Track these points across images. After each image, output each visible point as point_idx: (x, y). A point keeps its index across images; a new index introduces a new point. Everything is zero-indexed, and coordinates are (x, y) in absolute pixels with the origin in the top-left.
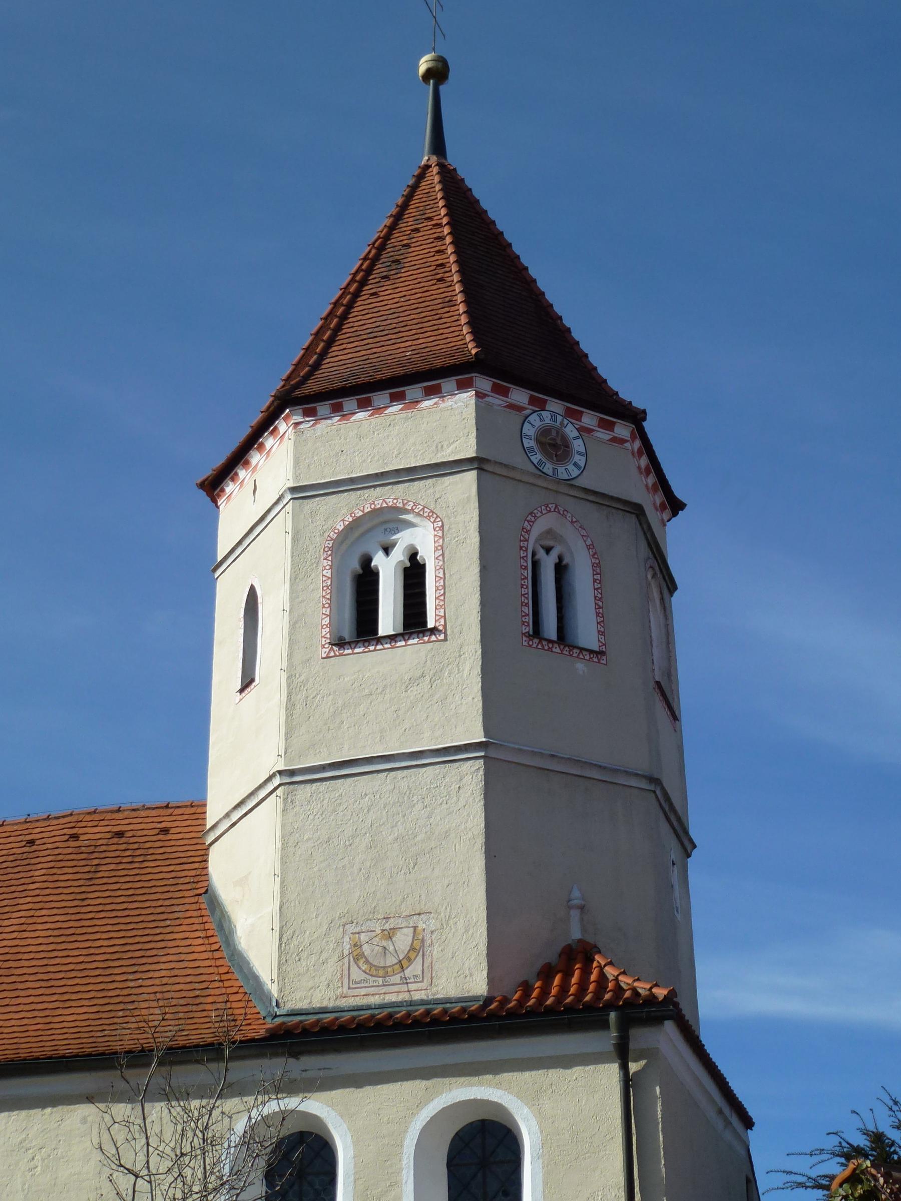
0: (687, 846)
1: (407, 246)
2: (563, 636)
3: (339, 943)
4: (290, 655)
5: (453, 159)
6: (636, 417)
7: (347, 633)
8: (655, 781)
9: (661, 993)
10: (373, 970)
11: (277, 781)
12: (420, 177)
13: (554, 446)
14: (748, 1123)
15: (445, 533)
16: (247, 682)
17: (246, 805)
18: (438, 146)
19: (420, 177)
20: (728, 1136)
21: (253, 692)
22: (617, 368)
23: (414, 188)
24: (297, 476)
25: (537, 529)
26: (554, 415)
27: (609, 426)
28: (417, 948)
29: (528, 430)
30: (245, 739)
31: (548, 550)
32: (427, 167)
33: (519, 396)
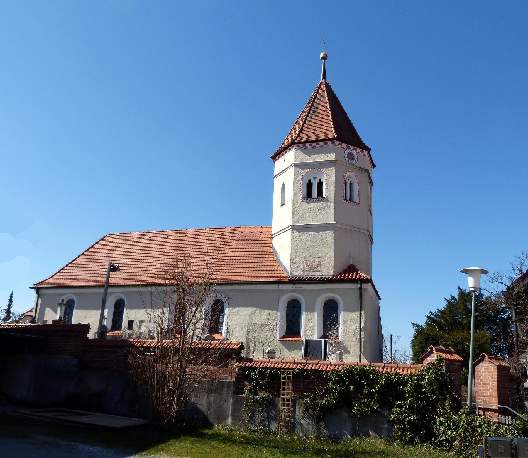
0: (372, 242)
1: (318, 104)
2: (351, 200)
3: (303, 262)
4: (293, 201)
5: (328, 80)
6: (368, 150)
7: (305, 196)
8: (368, 231)
9: (369, 277)
10: (310, 268)
11: (290, 228)
12: (321, 85)
13: (351, 157)
14: (380, 299)
15: (329, 179)
16: (282, 205)
17: (282, 231)
18: (324, 77)
19: (321, 85)
20: (376, 302)
21: (283, 207)
22: (366, 142)
23: (319, 88)
24: (295, 161)
25: (347, 176)
26: (351, 149)
27: (362, 152)
28: (319, 265)
29: (346, 153)
30: (282, 217)
31: (348, 180)
32: (322, 82)
33: (344, 145)
